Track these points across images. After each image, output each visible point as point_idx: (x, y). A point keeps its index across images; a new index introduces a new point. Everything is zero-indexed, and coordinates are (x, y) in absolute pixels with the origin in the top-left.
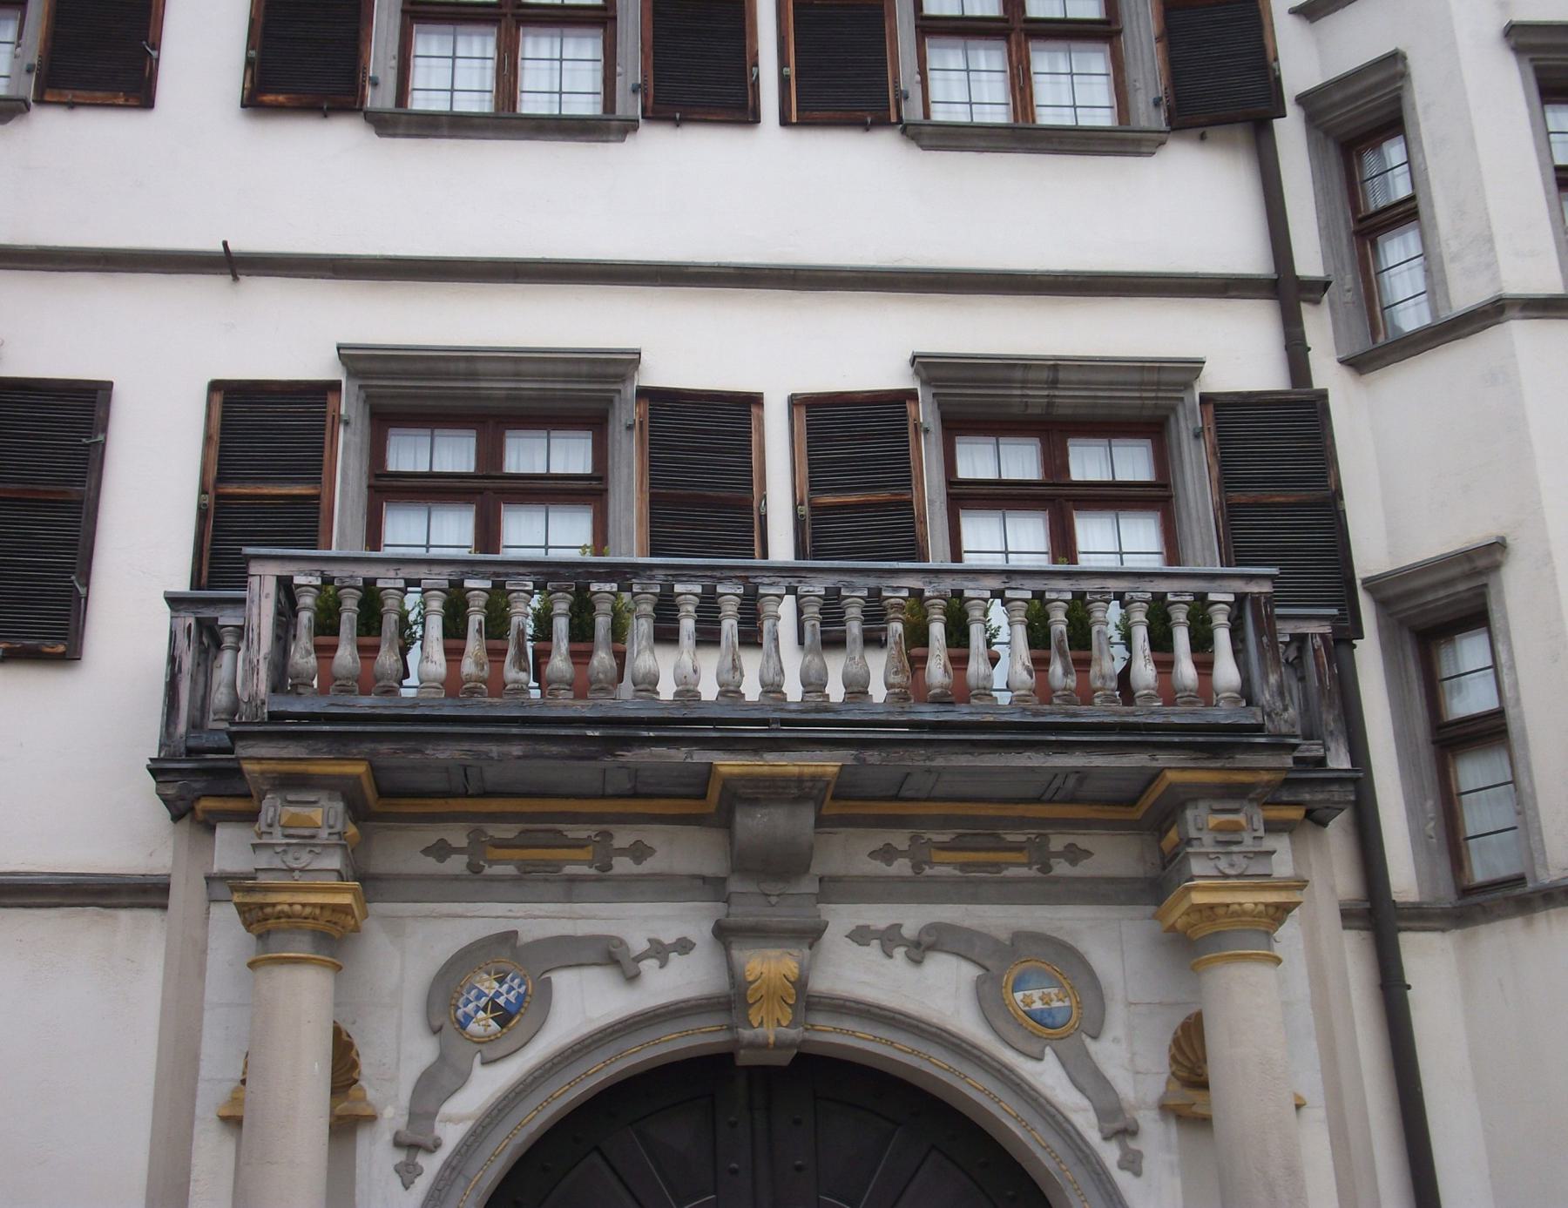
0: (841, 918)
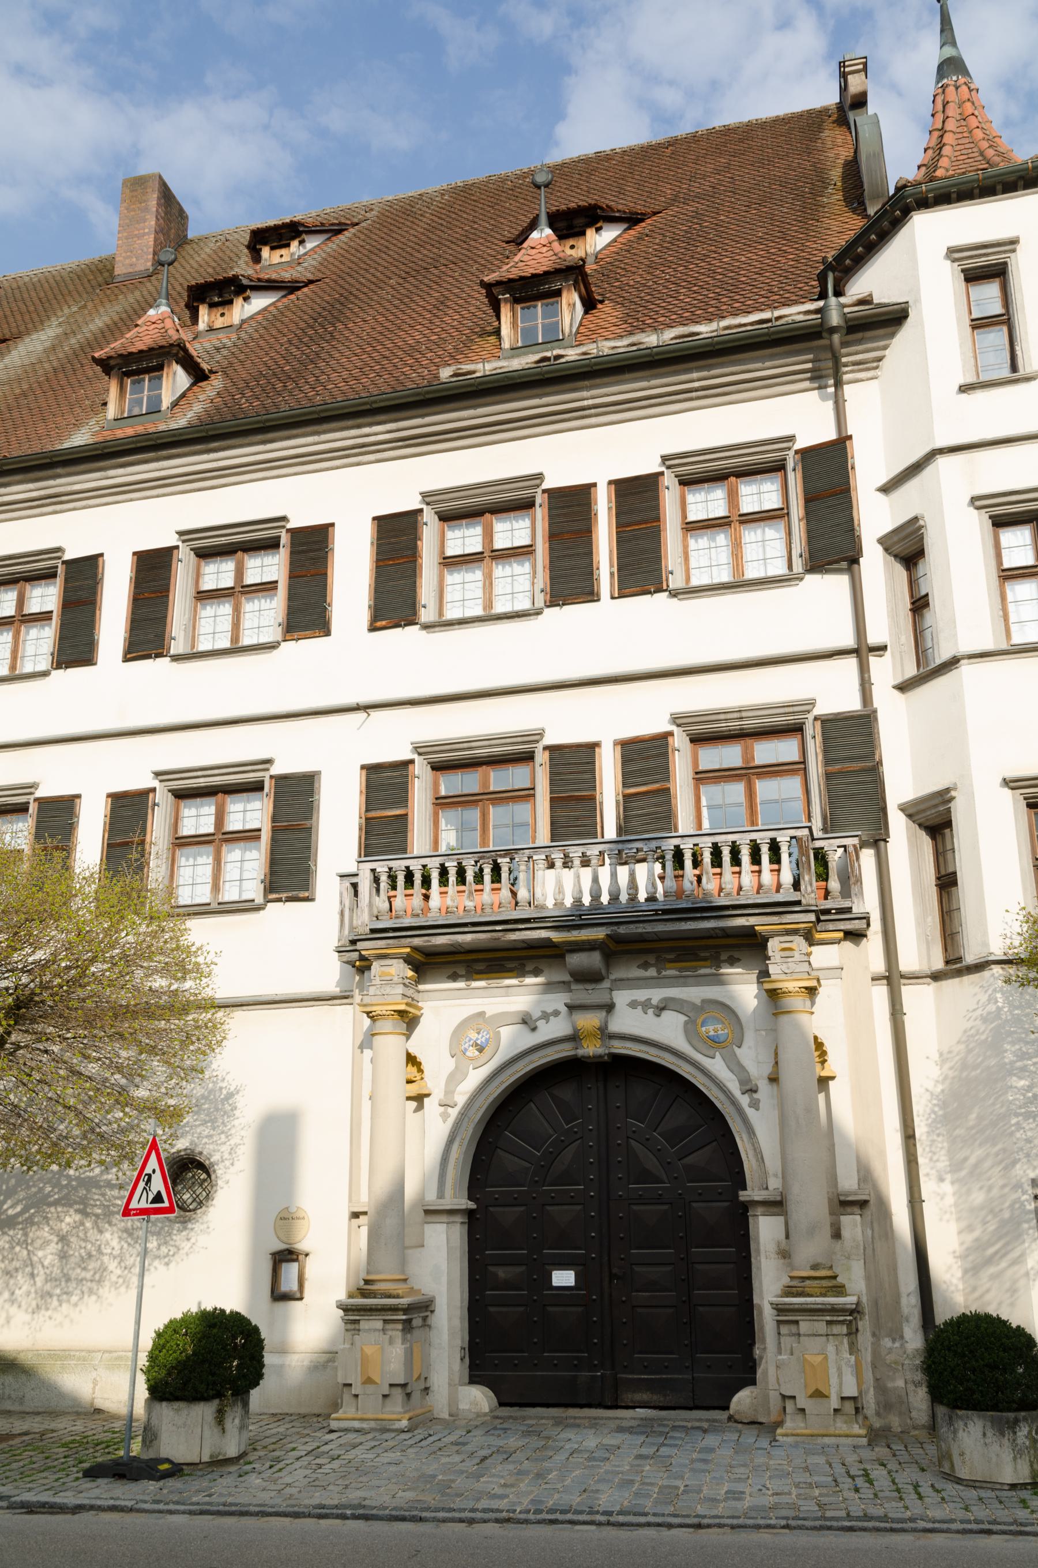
0: (622, 998)
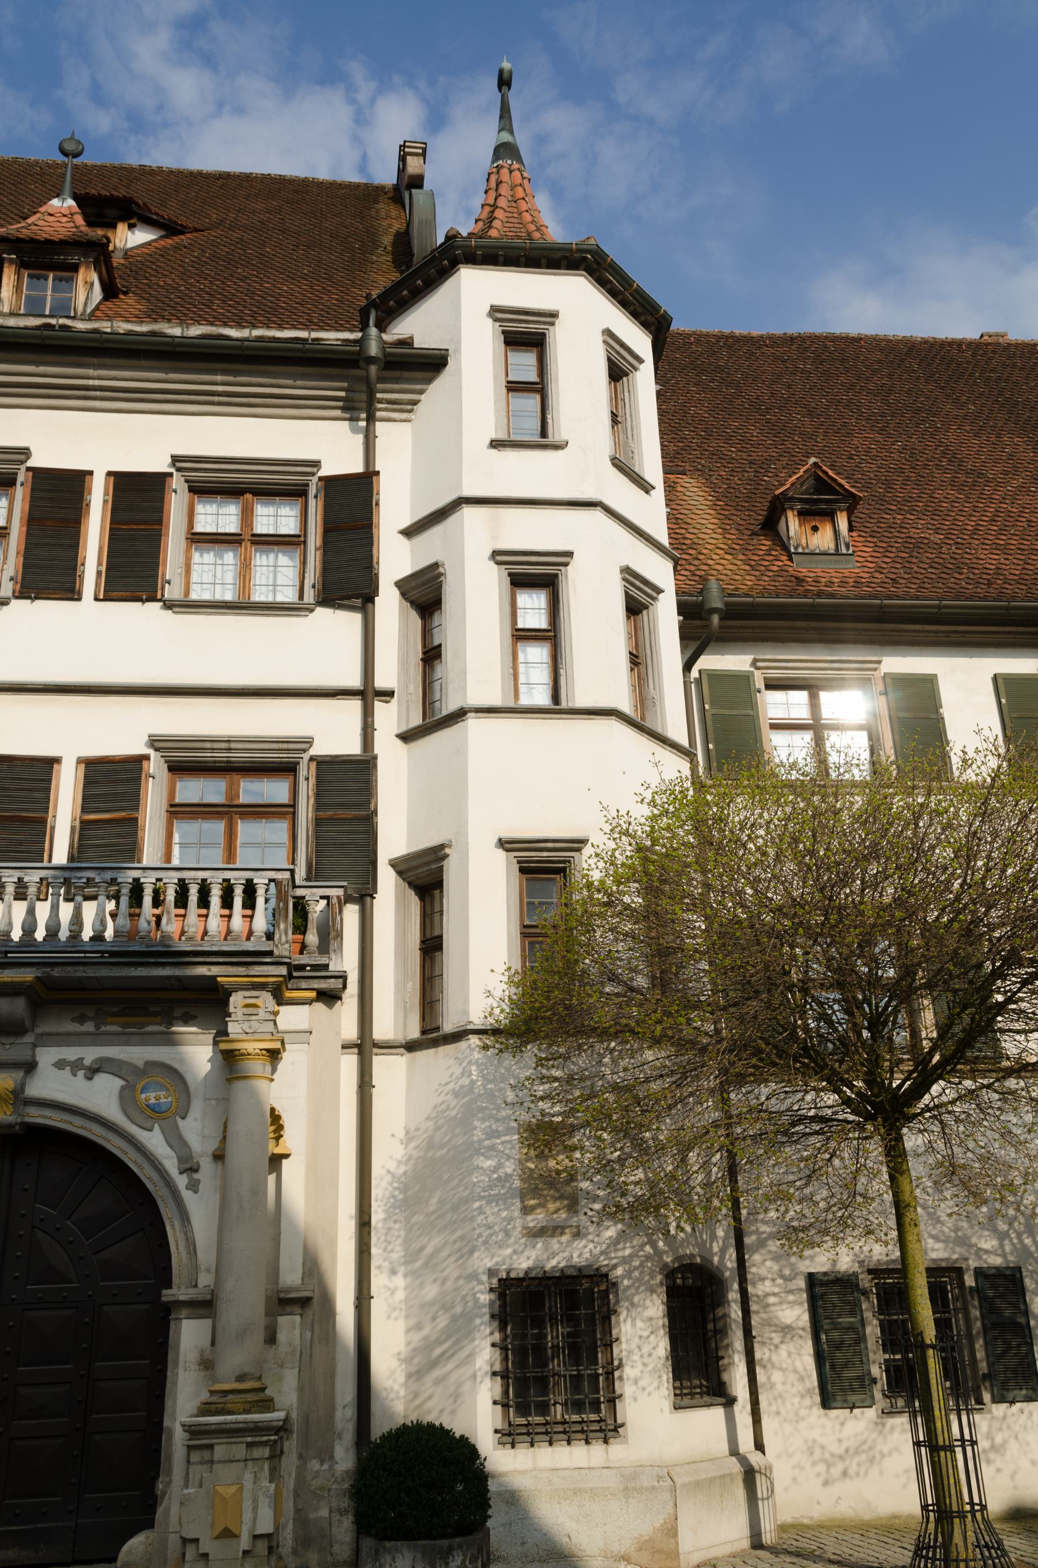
0: (47, 1056)
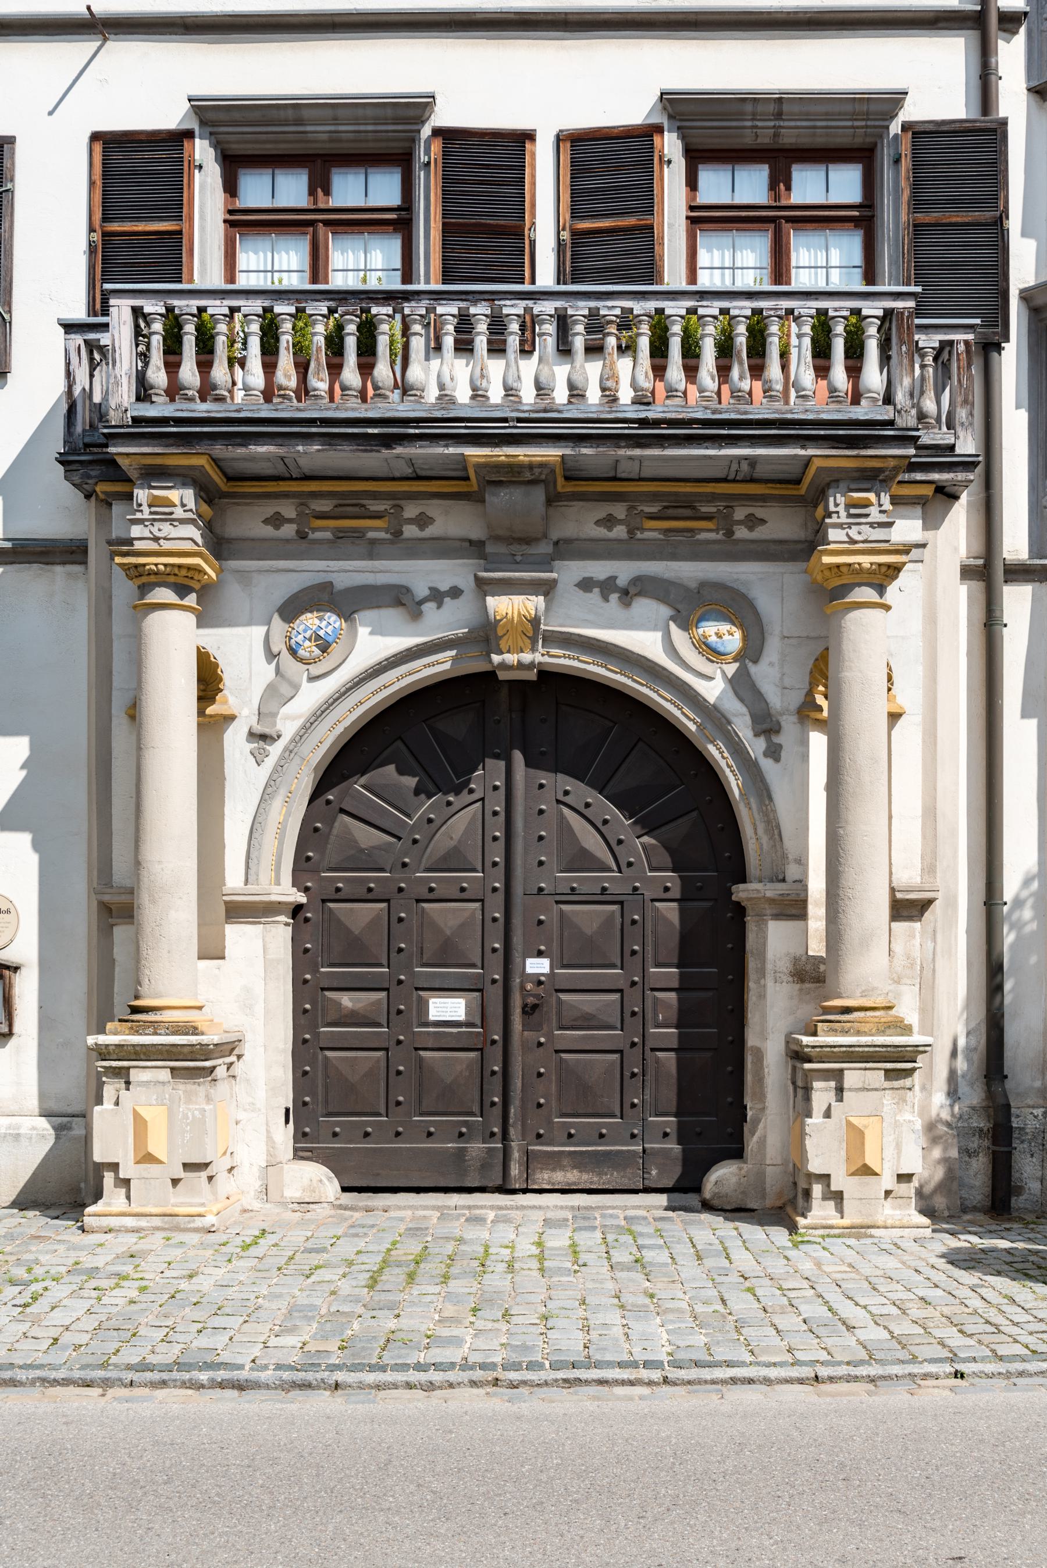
0: (569, 572)
